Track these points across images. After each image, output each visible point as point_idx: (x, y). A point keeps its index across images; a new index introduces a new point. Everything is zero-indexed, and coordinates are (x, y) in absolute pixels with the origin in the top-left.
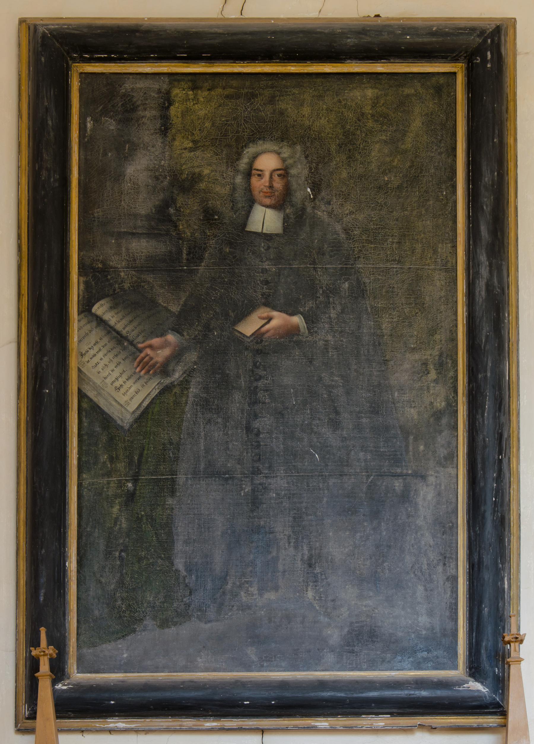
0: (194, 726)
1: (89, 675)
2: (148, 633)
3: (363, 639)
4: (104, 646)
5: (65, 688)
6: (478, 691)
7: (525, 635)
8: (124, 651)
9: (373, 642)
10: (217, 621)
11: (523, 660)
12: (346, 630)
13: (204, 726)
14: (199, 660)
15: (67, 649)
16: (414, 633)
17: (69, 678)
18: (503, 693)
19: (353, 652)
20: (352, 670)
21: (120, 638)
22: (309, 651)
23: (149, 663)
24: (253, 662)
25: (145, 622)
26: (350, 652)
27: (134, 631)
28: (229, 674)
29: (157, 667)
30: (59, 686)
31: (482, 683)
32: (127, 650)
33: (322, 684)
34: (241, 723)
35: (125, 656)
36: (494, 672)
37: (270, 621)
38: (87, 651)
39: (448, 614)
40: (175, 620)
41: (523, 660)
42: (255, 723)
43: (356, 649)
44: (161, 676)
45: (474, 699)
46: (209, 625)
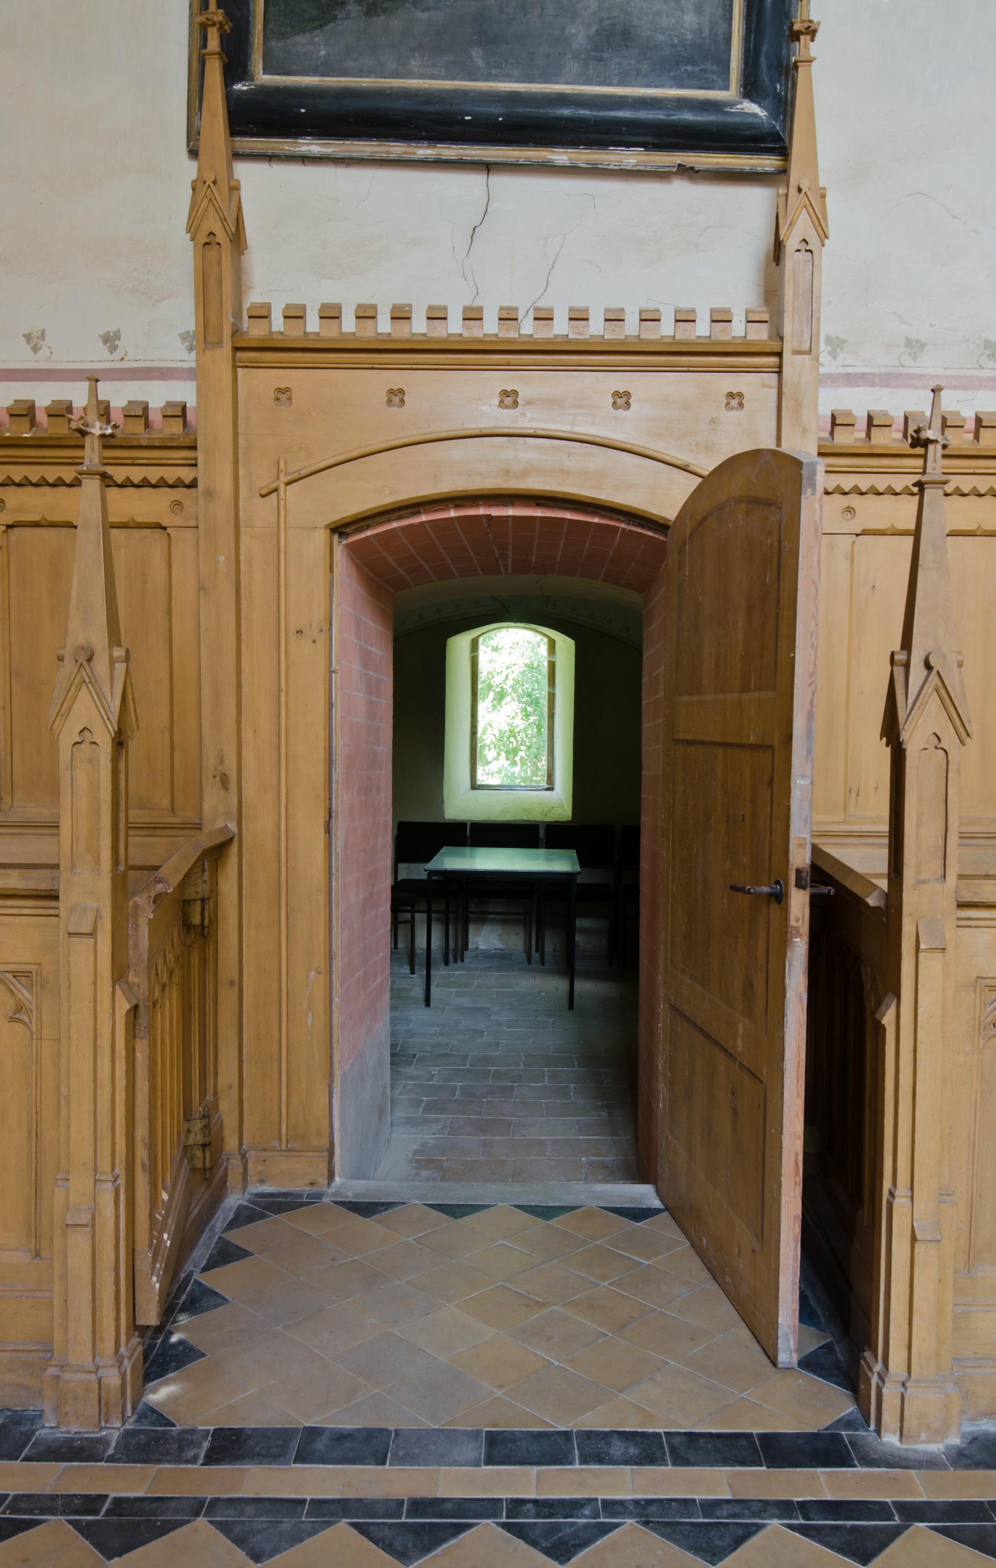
0: (404, 153)
1: (277, 77)
2: (351, 22)
3: (616, 41)
4: (297, 38)
5: (245, 88)
6: (754, 115)
7: (819, 23)
8: (322, 47)
9: (627, 46)
10: (437, 9)
11: (815, 59)
12: (594, 28)
13: (415, 154)
14: (413, 63)
15: (251, 40)
16: (677, 36)
17: (252, 80)
18: (784, 121)
19: (600, 59)
20: (600, 85)
21: (316, 29)
22: (548, 56)
23: (352, 64)
24: (479, 68)
25: (348, 7)
26: (597, 60)
27: (334, 19)
28: (449, 82)
29: (361, 71)
30: (238, 87)
31: (759, 104)
32: (325, 45)
33: (562, 99)
34: (461, 152)
35: (322, 53)
36: (776, 89)
37: (501, 12)
38: (275, 44)
39: (720, 11)
40: (385, 5)
41: (815, 59)
42: (478, 152)
43: (606, 55)
44: (365, 82)
45: (750, 126)
46: (426, 14)
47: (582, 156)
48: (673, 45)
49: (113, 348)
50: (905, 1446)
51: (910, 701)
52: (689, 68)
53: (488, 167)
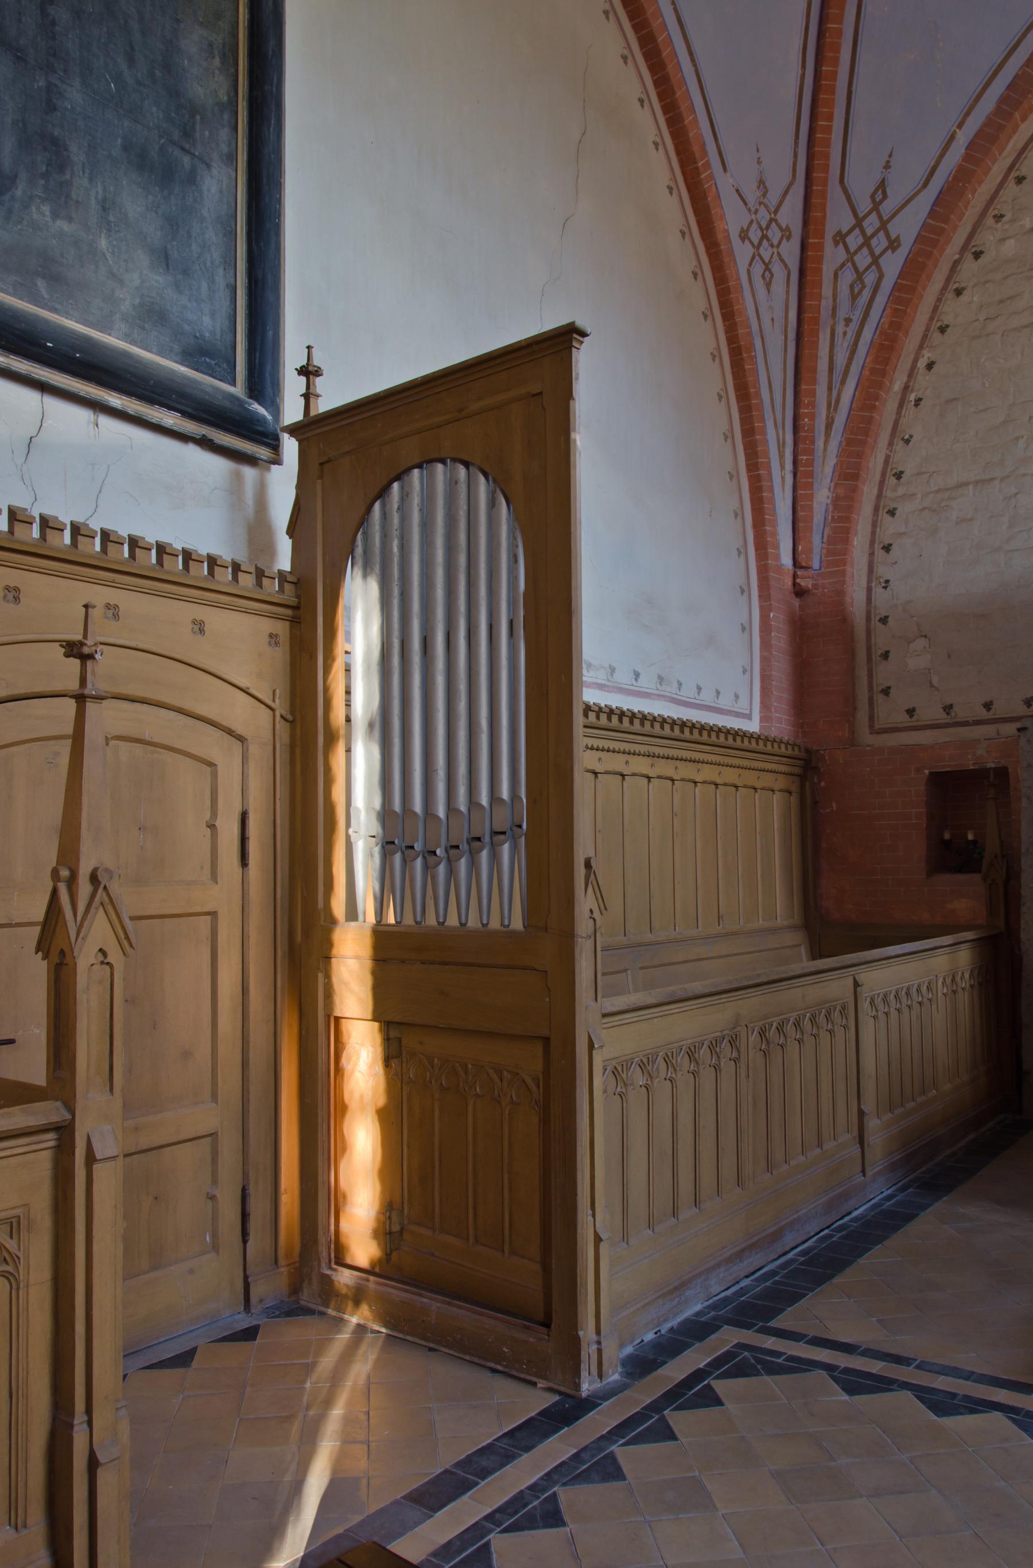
19: (143, 328)
31: (266, 409)
47: (133, 406)
48: (196, 337)
49: (911, 716)
50: (604, 1383)
51: (79, 918)
52: (208, 360)
53: (43, 387)
